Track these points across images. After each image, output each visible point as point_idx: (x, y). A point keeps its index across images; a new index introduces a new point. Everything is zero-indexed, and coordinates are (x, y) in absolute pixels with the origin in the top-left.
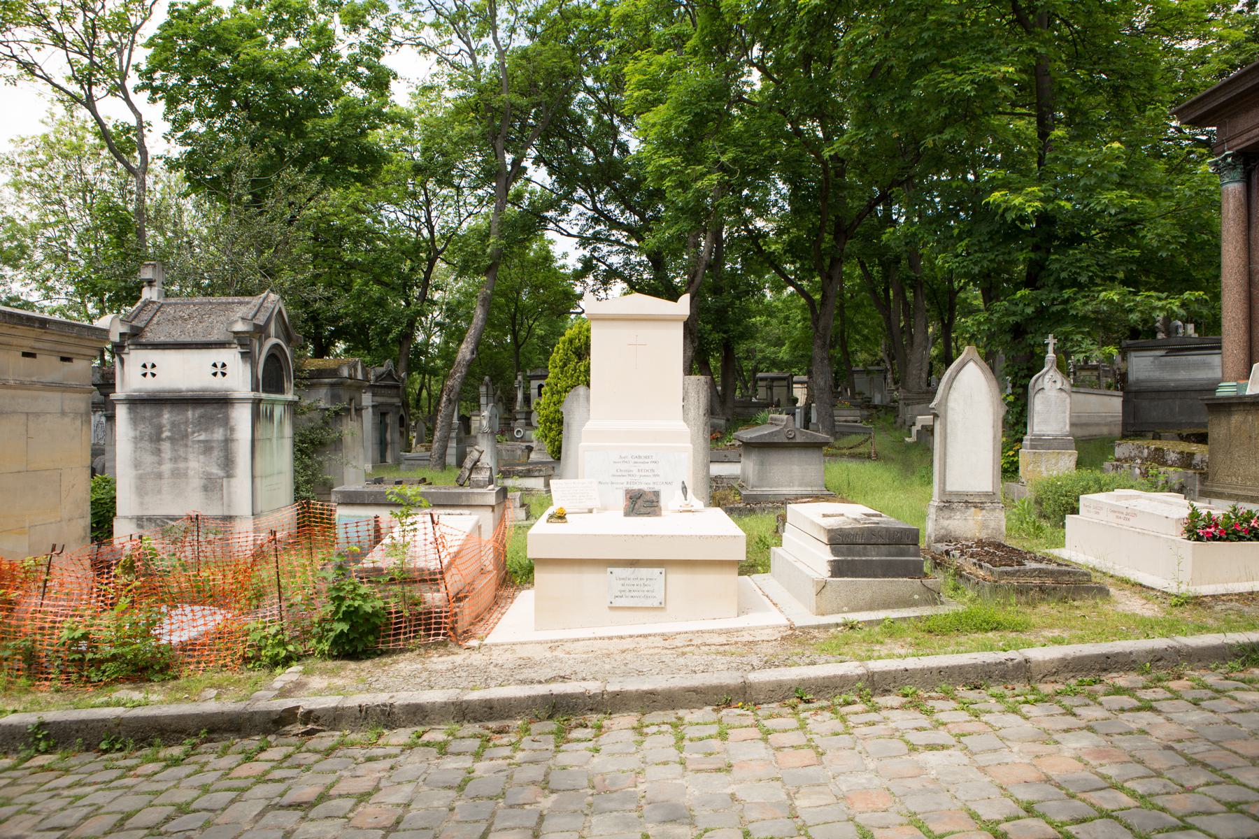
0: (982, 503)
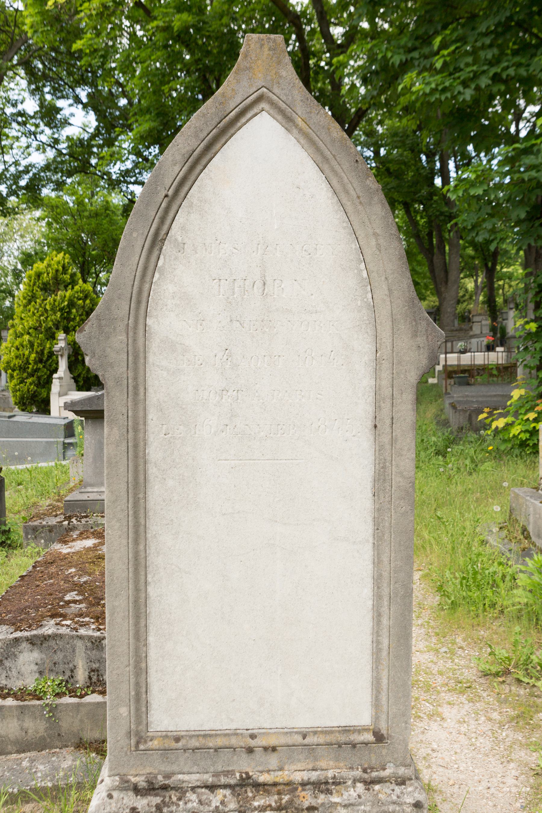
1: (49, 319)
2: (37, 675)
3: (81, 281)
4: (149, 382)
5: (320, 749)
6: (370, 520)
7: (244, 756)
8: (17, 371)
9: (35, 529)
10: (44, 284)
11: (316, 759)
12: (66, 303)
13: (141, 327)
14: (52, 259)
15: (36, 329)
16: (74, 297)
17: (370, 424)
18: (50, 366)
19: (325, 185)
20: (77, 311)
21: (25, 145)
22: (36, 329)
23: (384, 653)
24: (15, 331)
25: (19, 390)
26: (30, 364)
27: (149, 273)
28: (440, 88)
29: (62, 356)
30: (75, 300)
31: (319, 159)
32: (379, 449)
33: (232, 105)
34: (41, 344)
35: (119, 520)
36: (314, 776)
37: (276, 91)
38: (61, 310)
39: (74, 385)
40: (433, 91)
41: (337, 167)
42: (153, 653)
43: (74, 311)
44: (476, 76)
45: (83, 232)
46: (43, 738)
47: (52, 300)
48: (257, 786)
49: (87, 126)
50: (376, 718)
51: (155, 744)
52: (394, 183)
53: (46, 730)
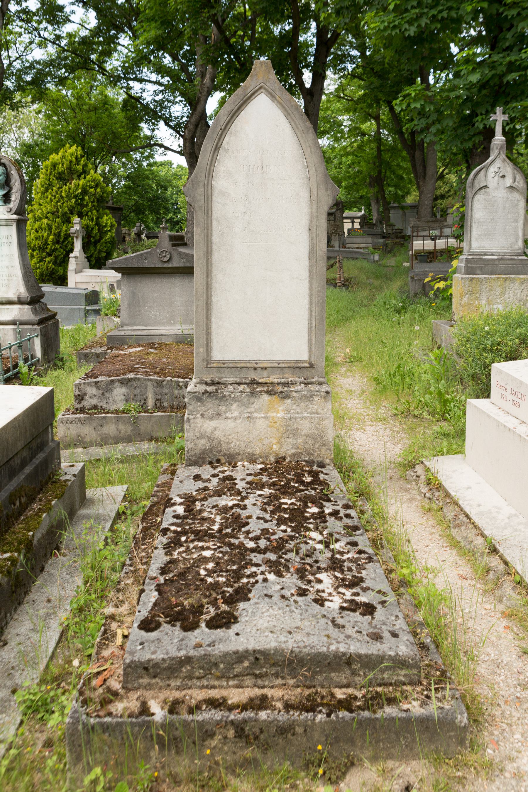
0: (286, 384)
1: (65, 205)
2: (125, 402)
3: (92, 172)
4: (213, 209)
5: (285, 370)
6: (307, 270)
7: (253, 371)
8: (37, 251)
9: (86, 356)
10: (59, 173)
11: (284, 374)
12: (80, 191)
13: (210, 185)
14: (66, 151)
15: (53, 213)
16: (87, 186)
17: (307, 228)
18: (66, 246)
19: (288, 125)
20: (89, 199)
21: (28, 40)
22: (53, 213)
23: (313, 328)
24: (34, 215)
25: (39, 268)
26: (49, 245)
27: (214, 162)
28: (391, 25)
29: (77, 237)
30: (88, 188)
31: (286, 114)
32: (312, 239)
33: (249, 90)
34: (58, 227)
35: (200, 267)
36: (283, 380)
37: (268, 84)
38: (76, 197)
39: (88, 264)
40: (386, 28)
41: (293, 117)
42: (214, 326)
43: (87, 198)
44: (419, 17)
45: (83, 124)
46: (130, 436)
47: (67, 187)
48: (258, 383)
49: (85, 22)
50: (310, 357)
51: (214, 365)
52: (376, 82)
53: (132, 431)
